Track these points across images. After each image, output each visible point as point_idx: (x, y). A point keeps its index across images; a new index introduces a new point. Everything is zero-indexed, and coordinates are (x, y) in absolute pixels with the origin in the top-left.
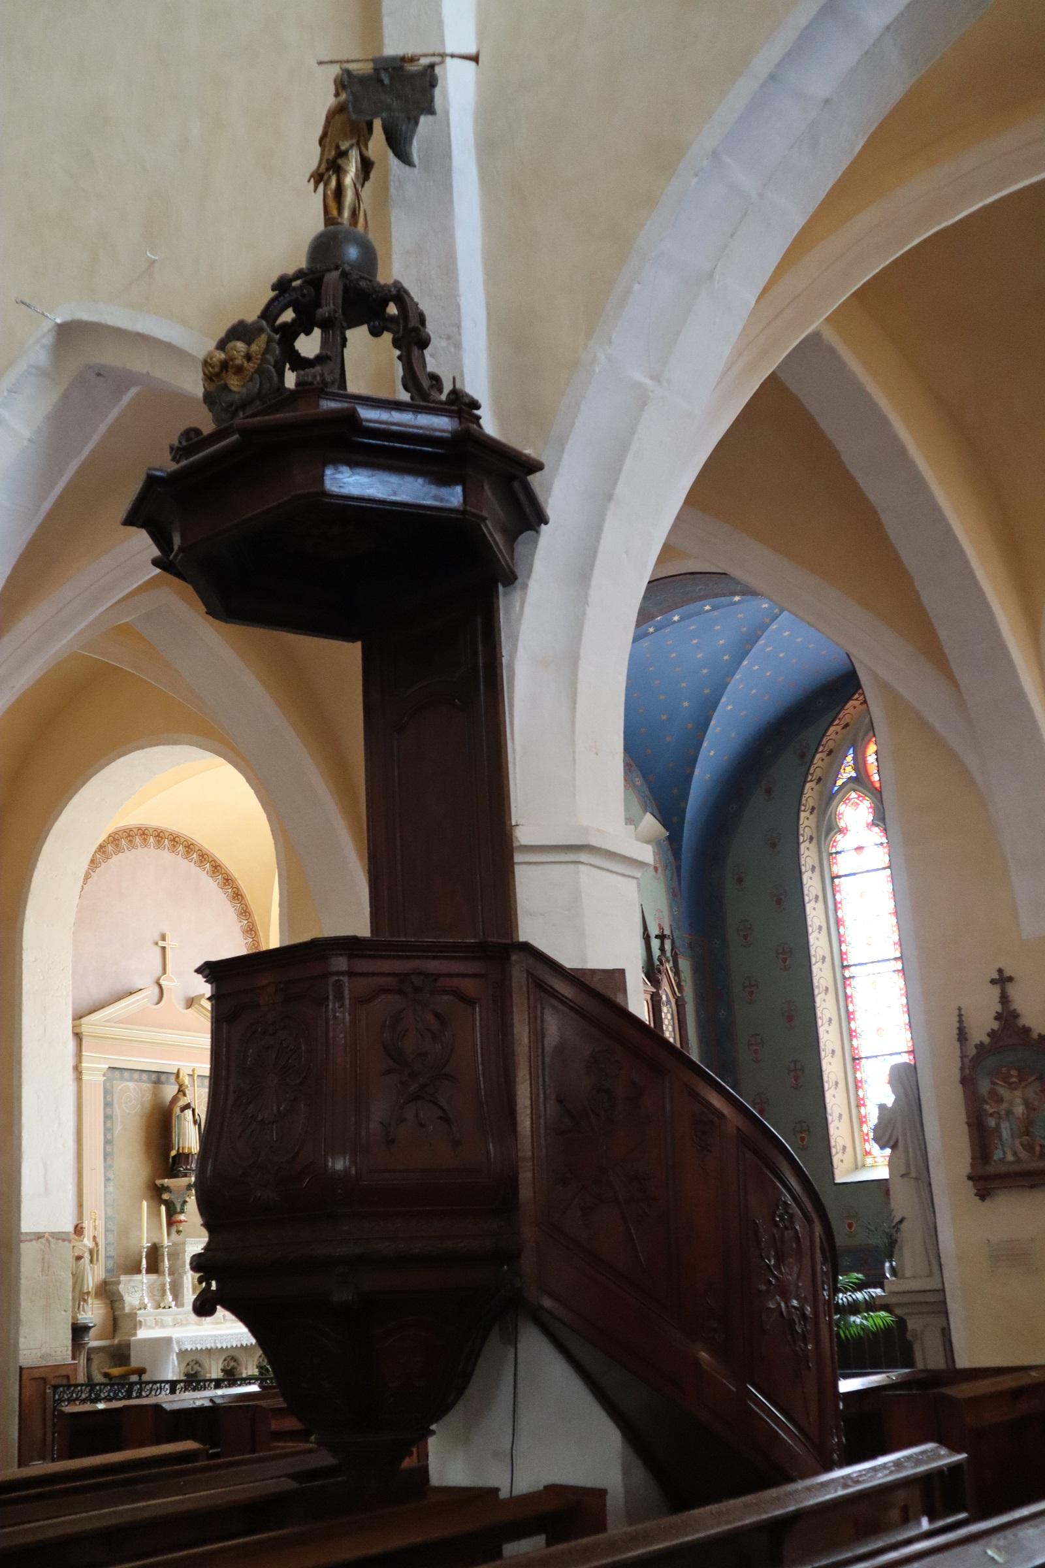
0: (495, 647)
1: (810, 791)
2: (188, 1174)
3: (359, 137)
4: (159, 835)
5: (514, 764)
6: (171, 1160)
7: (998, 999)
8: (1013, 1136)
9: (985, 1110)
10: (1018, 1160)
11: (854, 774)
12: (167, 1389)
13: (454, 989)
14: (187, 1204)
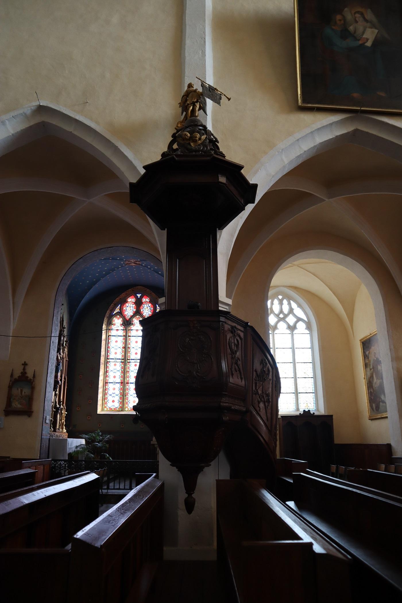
7: (23, 369)
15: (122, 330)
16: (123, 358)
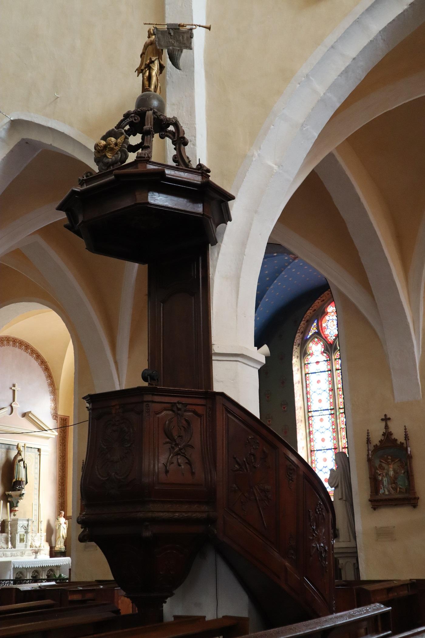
0: (207, 271)
1: (298, 339)
2: (20, 490)
3: (159, 56)
4: (14, 341)
5: (213, 319)
6: (13, 483)
8: (388, 484)
9: (377, 473)
10: (390, 493)
11: (317, 331)
12: (3, 583)
13: (193, 410)
14: (19, 503)
15: (324, 361)
16: (332, 408)
